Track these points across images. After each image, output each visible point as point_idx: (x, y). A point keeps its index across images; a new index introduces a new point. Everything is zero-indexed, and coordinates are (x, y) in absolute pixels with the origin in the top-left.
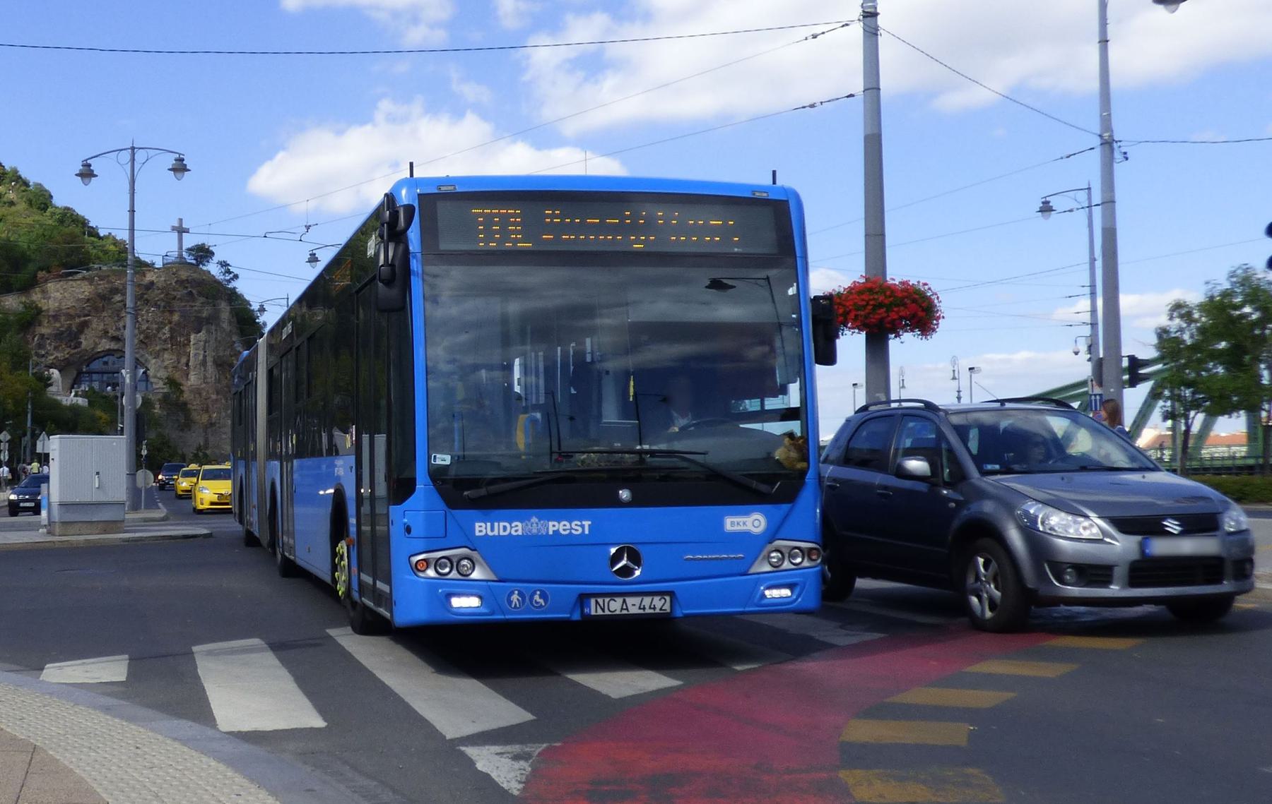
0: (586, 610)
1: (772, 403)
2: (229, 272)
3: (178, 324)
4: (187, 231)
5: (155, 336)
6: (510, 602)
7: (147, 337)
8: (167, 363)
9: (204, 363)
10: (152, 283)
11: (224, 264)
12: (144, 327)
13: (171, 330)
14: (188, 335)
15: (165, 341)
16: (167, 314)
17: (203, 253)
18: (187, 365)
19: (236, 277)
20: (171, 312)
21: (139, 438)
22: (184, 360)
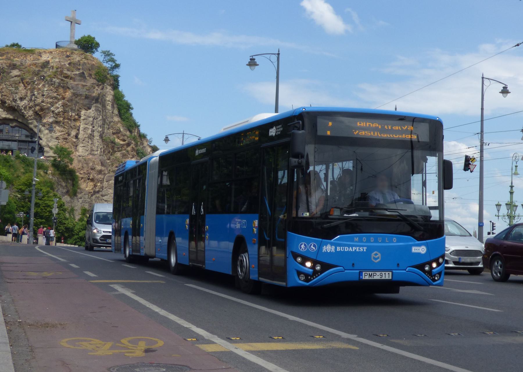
0: (361, 277)
1: (322, 176)
2: (113, 61)
3: (70, 100)
5: (48, 108)
6: (301, 248)
7: (42, 109)
8: (58, 134)
9: (91, 137)
10: (48, 62)
11: (107, 54)
13: (64, 105)
14: (79, 111)
15: (58, 114)
16: (61, 90)
18: (76, 137)
19: (117, 66)
20: (66, 88)
22: (73, 133)
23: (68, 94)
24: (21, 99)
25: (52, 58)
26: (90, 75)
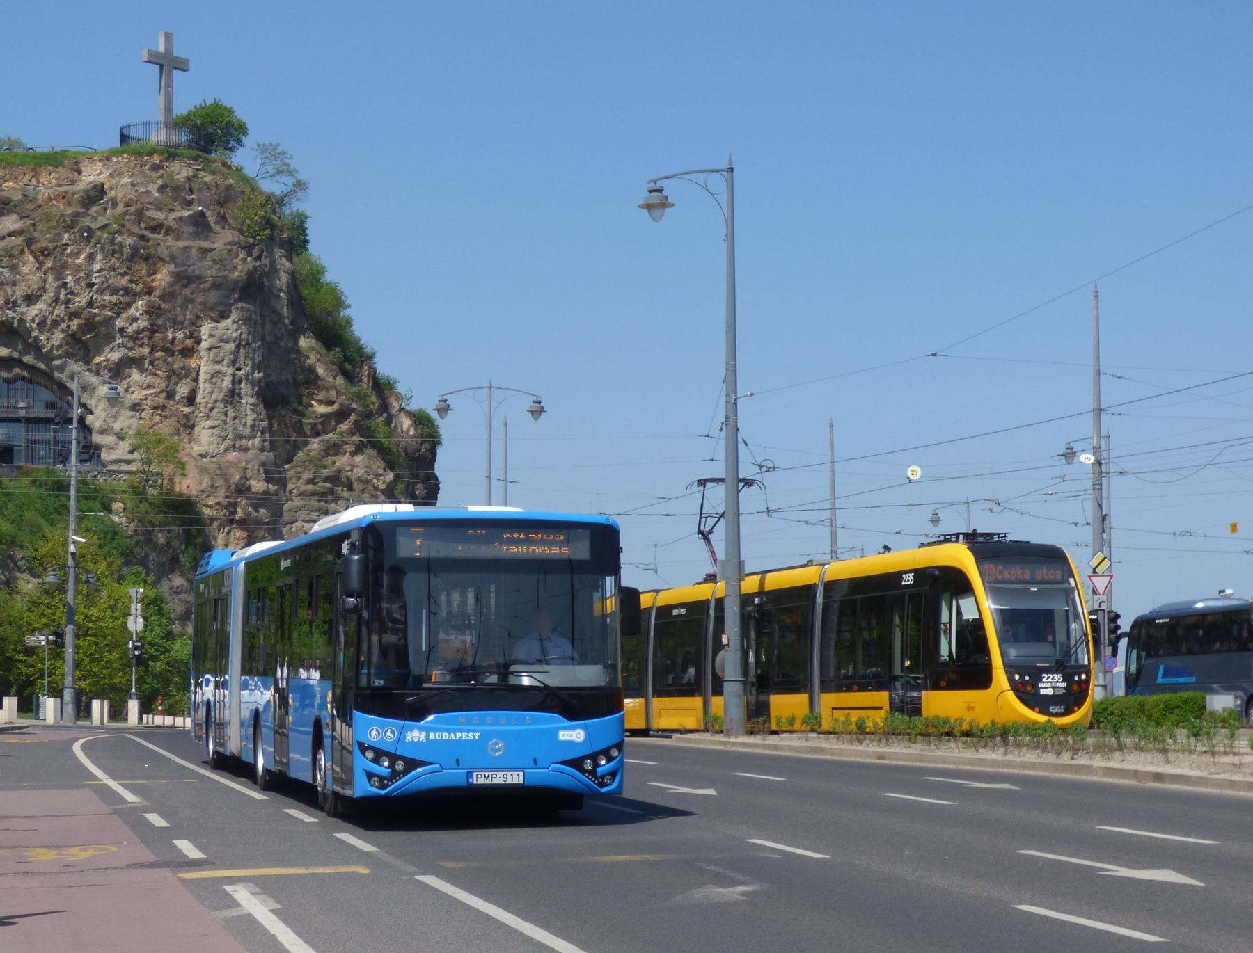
3: (168, 296)
4: (183, 66)
5: (108, 321)
8: (138, 395)
11: (270, 152)
12: (81, 301)
13: (151, 311)
14: (195, 323)
15: (135, 338)
17: (212, 132)
18: (191, 400)
19: (300, 185)
21: (919, 688)
23: (163, 277)
24: (30, 299)
25: (111, 175)
26: (222, 219)
